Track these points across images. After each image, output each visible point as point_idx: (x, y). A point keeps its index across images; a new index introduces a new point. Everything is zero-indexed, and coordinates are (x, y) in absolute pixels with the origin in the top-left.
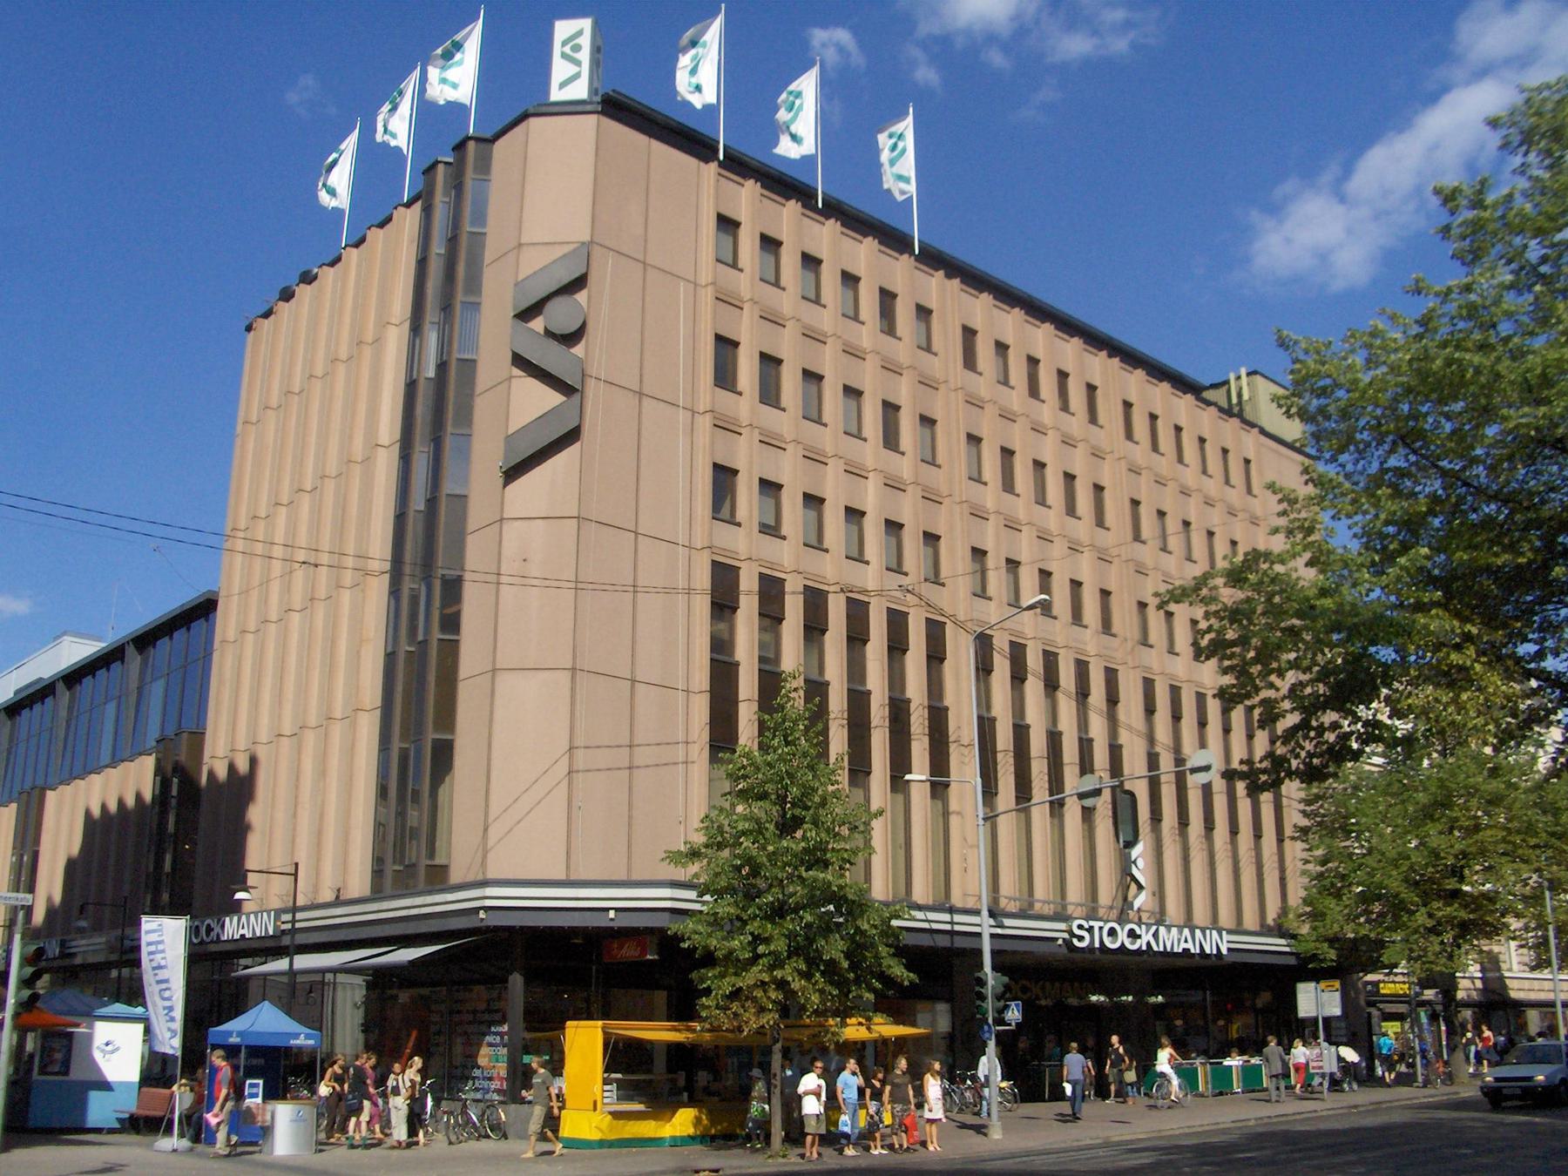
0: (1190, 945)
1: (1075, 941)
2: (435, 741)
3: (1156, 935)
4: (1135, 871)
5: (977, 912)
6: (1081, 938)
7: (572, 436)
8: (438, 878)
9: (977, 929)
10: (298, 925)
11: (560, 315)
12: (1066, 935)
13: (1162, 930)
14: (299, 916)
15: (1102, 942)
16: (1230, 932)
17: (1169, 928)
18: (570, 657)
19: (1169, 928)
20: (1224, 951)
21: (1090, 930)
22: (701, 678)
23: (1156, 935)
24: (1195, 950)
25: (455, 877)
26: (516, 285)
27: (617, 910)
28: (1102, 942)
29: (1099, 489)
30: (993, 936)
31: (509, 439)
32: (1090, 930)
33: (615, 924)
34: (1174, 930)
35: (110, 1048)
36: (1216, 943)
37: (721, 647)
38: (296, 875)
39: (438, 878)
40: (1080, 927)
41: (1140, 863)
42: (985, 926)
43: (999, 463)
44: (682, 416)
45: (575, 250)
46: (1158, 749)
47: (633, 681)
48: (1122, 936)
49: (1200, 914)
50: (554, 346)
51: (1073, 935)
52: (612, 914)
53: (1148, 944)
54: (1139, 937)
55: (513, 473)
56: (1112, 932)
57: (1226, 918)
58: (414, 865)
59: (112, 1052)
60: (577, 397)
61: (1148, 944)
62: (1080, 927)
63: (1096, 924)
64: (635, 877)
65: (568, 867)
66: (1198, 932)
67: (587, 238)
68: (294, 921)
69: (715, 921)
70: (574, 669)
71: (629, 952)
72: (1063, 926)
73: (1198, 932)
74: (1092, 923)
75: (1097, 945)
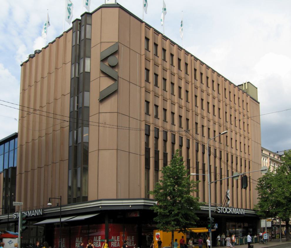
0: (34, 214)
1: (218, 211)
2: (83, 167)
3: (232, 210)
4: (228, 196)
5: (208, 206)
6: (219, 211)
7: (115, 92)
8: (85, 199)
9: (208, 209)
10: (62, 210)
11: (112, 61)
12: (216, 210)
13: (233, 209)
14: (62, 208)
15: (223, 212)
16: (245, 209)
17: (234, 208)
18: (101, 149)
19: (234, 208)
20: (244, 214)
21: (221, 209)
22: (143, 152)
23: (232, 210)
24: (34, 215)
25: (90, 199)
26: (101, 53)
27: (131, 205)
28: (223, 212)
29: (188, 120)
30: (211, 211)
31: (100, 93)
32: (221, 209)
33: (131, 209)
34: (235, 209)
35: (11, 242)
36: (243, 212)
37: (147, 144)
38: (61, 199)
39: (85, 199)
40: (219, 208)
41: (229, 194)
42: (210, 209)
43: (207, 105)
44: (138, 88)
45: (115, 44)
46: (233, 171)
47: (129, 152)
48: (226, 210)
49: (239, 206)
50: (111, 69)
51: (217, 210)
52: (130, 206)
53: (231, 212)
54: (229, 210)
55: (102, 101)
56: (225, 209)
57: (244, 207)
58: (79, 197)
59: (11, 243)
60: (117, 81)
61: (231, 212)
62: (219, 208)
63: (222, 208)
64: (130, 198)
65: (117, 196)
66: (239, 209)
67: (117, 41)
68: (61, 209)
69: (160, 207)
70: (117, 149)
71: (133, 215)
72: (215, 208)
73: (239, 209)
74: (221, 207)
75: (222, 212)
